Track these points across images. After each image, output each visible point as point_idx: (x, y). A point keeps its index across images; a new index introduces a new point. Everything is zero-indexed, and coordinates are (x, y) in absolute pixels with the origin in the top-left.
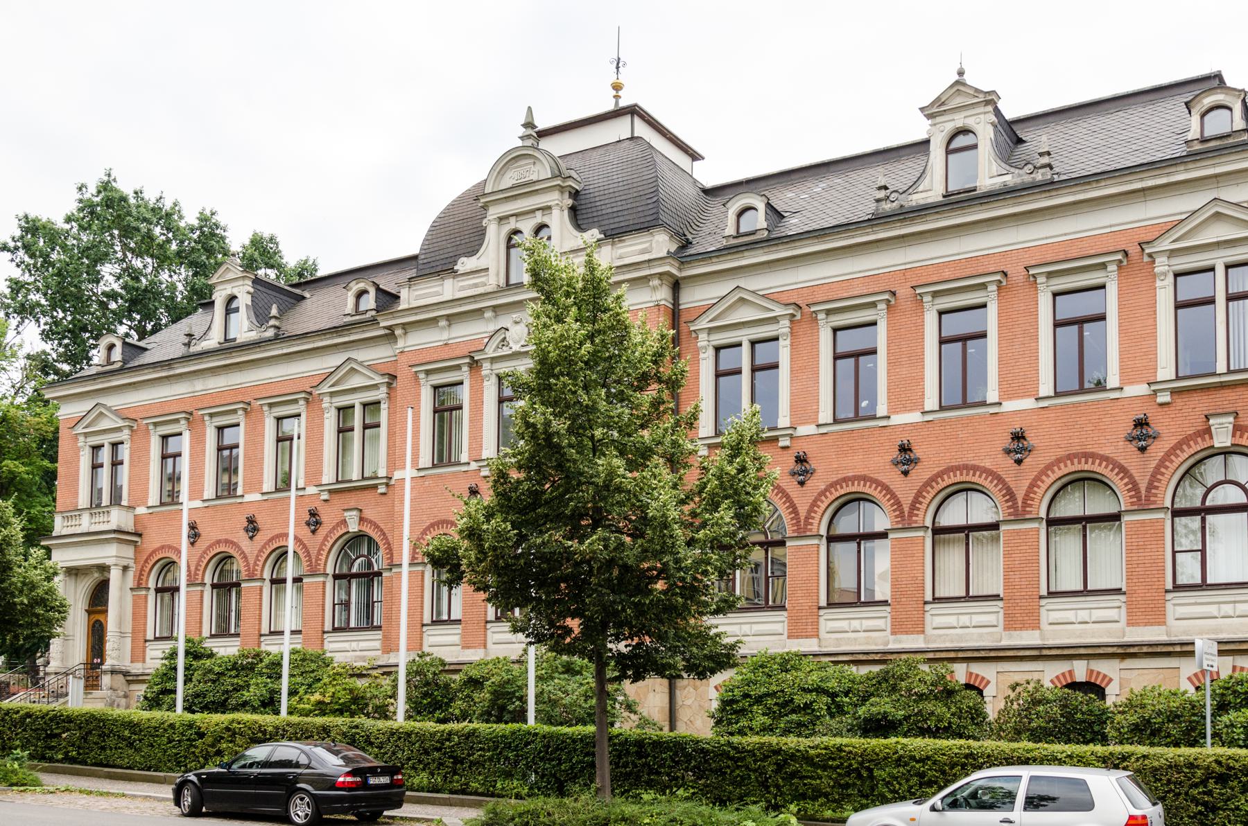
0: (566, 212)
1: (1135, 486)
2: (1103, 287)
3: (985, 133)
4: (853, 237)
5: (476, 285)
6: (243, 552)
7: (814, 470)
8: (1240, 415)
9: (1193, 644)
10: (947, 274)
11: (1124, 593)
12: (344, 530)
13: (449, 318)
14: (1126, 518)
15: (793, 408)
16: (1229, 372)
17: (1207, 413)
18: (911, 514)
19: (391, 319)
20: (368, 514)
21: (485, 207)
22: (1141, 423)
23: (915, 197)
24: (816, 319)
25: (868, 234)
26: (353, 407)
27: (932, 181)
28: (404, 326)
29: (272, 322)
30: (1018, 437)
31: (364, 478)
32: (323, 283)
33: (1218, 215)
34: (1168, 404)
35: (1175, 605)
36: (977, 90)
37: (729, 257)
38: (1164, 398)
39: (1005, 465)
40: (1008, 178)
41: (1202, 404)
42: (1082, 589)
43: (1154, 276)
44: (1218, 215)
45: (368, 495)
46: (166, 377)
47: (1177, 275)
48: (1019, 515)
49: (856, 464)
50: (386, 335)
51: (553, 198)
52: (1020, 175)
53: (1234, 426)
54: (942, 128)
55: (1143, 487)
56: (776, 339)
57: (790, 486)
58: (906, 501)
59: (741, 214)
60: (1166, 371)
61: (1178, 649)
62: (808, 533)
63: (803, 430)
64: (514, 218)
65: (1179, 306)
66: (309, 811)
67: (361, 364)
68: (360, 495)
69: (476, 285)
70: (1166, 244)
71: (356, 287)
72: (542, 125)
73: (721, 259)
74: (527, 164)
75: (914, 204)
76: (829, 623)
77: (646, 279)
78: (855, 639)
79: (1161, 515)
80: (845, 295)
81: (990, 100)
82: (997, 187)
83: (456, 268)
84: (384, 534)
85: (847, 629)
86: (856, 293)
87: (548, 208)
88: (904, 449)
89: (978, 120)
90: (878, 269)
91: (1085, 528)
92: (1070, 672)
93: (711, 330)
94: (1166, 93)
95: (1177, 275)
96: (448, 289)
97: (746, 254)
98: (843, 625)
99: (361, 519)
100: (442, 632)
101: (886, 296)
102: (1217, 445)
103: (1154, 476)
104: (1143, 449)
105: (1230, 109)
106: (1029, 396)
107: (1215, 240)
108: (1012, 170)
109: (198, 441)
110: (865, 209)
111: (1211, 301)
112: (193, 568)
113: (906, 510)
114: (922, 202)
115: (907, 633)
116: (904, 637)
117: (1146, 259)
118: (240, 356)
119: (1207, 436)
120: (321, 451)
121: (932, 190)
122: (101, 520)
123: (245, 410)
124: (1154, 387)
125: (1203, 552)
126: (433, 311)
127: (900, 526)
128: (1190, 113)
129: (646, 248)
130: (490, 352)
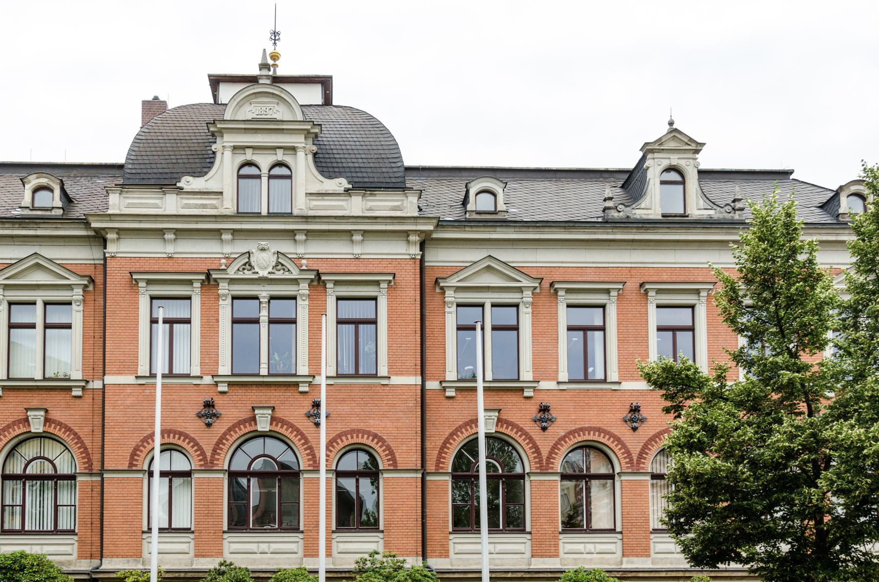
1: (203, 454)
2: (189, 298)
4: (595, 233)
5: (204, 206)
7: (221, 414)
8: (276, 410)
9: (481, 572)
10: (665, 278)
11: (193, 532)
12: (252, 429)
13: (178, 232)
14: (195, 476)
15: (536, 367)
16: (270, 375)
17: (253, 405)
18: (639, 462)
19: (107, 221)
20: (55, 415)
21: (221, 132)
22: (209, 405)
23: (638, 212)
25: (608, 233)
27: (651, 201)
28: (119, 231)
30: (635, 410)
31: (45, 379)
32: (710, 176)
33: (38, 265)
34: (305, 393)
35: (230, 542)
36: (691, 140)
37: (482, 229)
38: (223, 388)
40: (712, 212)
43: (218, 296)
44: (38, 265)
45: (58, 397)
48: (208, 466)
49: (591, 418)
50: (88, 237)
51: (298, 140)
52: (721, 213)
53: (272, 417)
54: (659, 163)
55: (209, 454)
57: (534, 430)
58: (635, 452)
60: (224, 369)
62: (550, 471)
63: (544, 385)
64: (282, 150)
65: (235, 321)
68: (44, 395)
69: (204, 206)
70: (453, 282)
71: (34, 181)
72: (282, 71)
73: (474, 229)
74: (273, 103)
75: (638, 217)
77: (407, 233)
78: (591, 560)
80: (580, 279)
82: (705, 217)
83: (178, 185)
84: (79, 438)
85: (256, 551)
86: (589, 279)
87: (293, 149)
88: (635, 410)
89: (688, 163)
90: (609, 263)
93: (458, 289)
94: (756, 177)
95: (234, 298)
96: (170, 204)
97: (498, 229)
98: (253, 547)
99: (47, 420)
100: (345, 540)
102: (259, 429)
104: (209, 425)
105: (494, 195)
108: (715, 207)
109: (317, 313)
110: (594, 212)
111: (256, 321)
113: (635, 458)
114: (645, 217)
115: (637, 556)
116: (635, 559)
117: (438, 290)
118: (64, 229)
119: (253, 423)
124: (216, 379)
126: (162, 222)
127: (630, 471)
128: (24, 186)
129: (398, 206)
130: (232, 273)
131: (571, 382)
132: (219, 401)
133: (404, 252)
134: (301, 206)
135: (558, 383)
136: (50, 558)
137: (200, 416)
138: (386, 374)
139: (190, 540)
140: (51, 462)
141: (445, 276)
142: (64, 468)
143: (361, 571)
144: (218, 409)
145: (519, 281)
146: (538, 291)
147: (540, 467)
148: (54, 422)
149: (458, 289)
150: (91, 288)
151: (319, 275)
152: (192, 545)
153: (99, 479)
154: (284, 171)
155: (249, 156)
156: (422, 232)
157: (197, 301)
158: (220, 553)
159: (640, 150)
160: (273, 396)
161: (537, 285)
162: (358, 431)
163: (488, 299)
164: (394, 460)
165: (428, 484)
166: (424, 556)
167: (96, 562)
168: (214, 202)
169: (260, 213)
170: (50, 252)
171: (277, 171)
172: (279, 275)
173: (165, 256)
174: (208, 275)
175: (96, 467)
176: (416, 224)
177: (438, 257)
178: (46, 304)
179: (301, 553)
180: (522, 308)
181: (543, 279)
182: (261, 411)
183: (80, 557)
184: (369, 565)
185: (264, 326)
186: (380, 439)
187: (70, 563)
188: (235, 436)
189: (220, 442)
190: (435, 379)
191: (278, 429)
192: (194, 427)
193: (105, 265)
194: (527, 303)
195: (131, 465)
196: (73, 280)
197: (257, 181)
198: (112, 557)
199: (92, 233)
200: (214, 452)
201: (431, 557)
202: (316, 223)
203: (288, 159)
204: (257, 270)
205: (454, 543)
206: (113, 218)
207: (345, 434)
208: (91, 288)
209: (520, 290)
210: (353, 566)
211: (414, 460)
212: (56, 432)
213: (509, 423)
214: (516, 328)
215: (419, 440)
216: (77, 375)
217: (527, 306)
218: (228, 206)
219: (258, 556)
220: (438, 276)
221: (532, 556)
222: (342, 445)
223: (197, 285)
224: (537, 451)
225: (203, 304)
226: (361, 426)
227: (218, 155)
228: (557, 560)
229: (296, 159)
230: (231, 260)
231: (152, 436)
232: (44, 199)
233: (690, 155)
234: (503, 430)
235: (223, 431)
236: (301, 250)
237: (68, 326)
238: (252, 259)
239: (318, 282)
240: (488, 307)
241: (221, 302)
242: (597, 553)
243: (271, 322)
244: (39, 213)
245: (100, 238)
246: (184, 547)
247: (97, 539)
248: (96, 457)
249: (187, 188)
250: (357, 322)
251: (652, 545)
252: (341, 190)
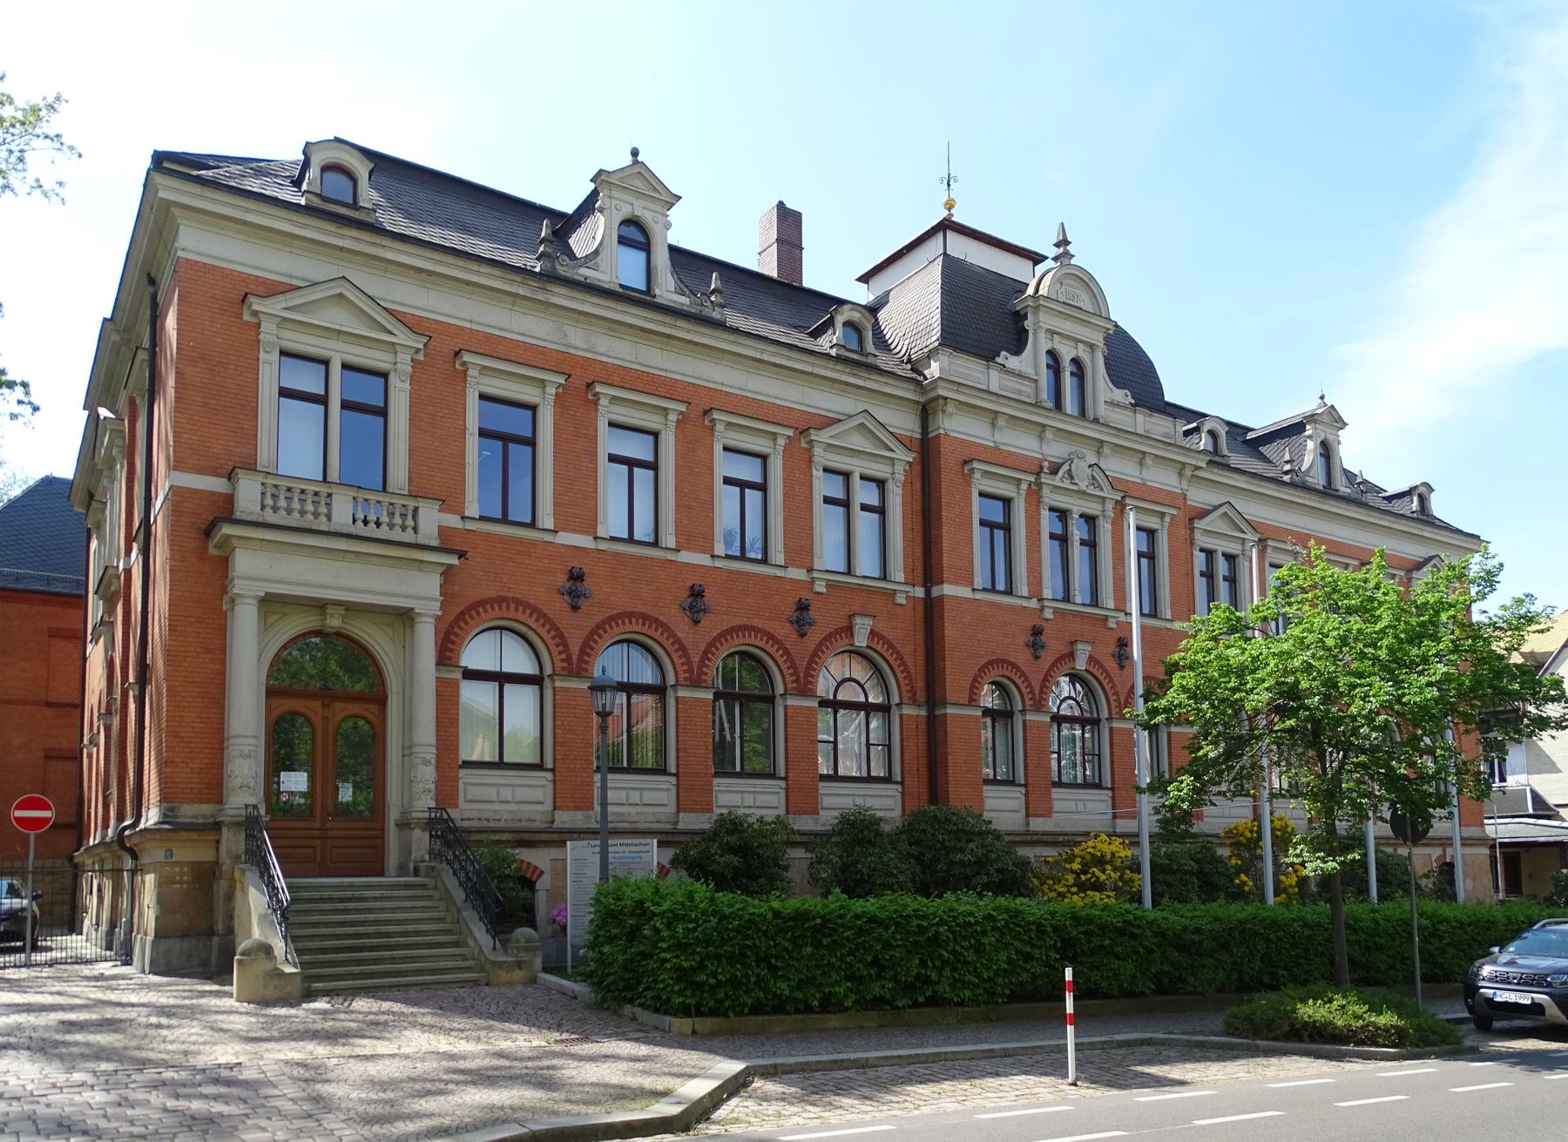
6: (678, 641)
34: (822, 594)
39: (557, 607)
42: (497, 760)
46: (835, 381)
55: (575, 650)
57: (682, 627)
103: (706, 652)
105: (354, 180)
106: (803, 567)
107: (338, 328)
131: (482, 518)
139: (545, 783)
145: (1244, 532)
159: (591, 181)
161: (421, 346)
173: (992, 444)
181: (570, 376)
205: (465, 784)
206: (960, 389)
214: (382, 412)
217: (403, 378)
220: (247, 291)
233: (658, 208)
240: (336, 369)
242: (644, 805)
251: (461, 786)
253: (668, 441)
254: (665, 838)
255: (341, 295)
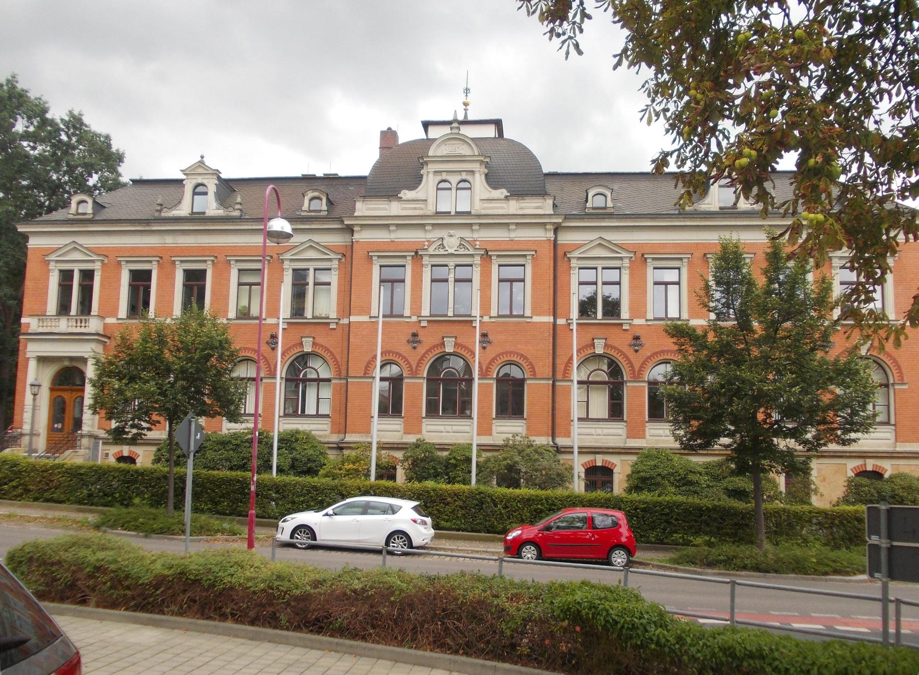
0: (483, 176)
1: (410, 366)
2: (404, 266)
3: (212, 188)
5: (415, 209)
12: (592, 351)
13: (397, 225)
15: (632, 309)
16: (455, 316)
20: (319, 340)
22: (415, 335)
24: (175, 264)
26: (309, 270)
28: (362, 226)
29: (238, 206)
33: (75, 248)
34: (425, 327)
38: (424, 324)
41: (444, 329)
43: (422, 266)
44: (311, 246)
47: (432, 266)
50: (342, 229)
51: (476, 167)
55: (414, 367)
56: (330, 269)
57: (630, 352)
59: (311, 199)
60: (426, 312)
61: (611, 451)
63: (637, 322)
65: (433, 281)
66: (535, 552)
67: (81, 245)
69: (415, 209)
76: (498, 428)
77: (545, 224)
78: (668, 441)
79: (421, 381)
81: (216, 173)
84: (333, 355)
87: (473, 172)
91: (588, 387)
92: (122, 451)
93: (579, 258)
95: (432, 266)
96: (394, 208)
98: (442, 428)
99: (314, 344)
100: (615, 427)
101: (212, 258)
104: (415, 348)
105: (606, 196)
111: (446, 281)
112: (484, 368)
114: (707, 210)
117: (566, 259)
120: (279, 296)
121: (184, 210)
122: (49, 324)
123: (213, 261)
125: (588, 402)
126: (388, 220)
130: (431, 251)
132: (421, 333)
133: (543, 235)
134: (478, 208)
135: (490, 317)
136: (313, 433)
137: (408, 341)
138: (530, 315)
140: (316, 370)
141: (571, 250)
142: (324, 374)
143: (506, 446)
144: (420, 338)
146: (633, 259)
147: (412, 374)
148: (318, 345)
149: (579, 258)
150: (343, 260)
151: (487, 251)
152: (402, 426)
153: (345, 382)
154: (466, 185)
155: (444, 176)
156: (554, 223)
157: (409, 269)
158: (420, 432)
160: (457, 329)
162: (511, 353)
163: (600, 264)
164: (902, 379)
165: (557, 387)
166: (553, 436)
167: (342, 436)
168: (421, 206)
169: (204, 213)
170: (317, 238)
171: (462, 185)
172: (462, 252)
173: (545, 239)
174: (416, 253)
175: (344, 373)
176: (550, 218)
177: (565, 238)
178: (315, 270)
179: (624, 436)
180: (623, 271)
182: (448, 339)
183: (332, 432)
184: (511, 442)
185: (451, 283)
186: (525, 358)
187: (325, 436)
188: (431, 355)
189: (422, 359)
190: (563, 318)
191: (459, 351)
192: (405, 349)
193: (352, 246)
194: (626, 267)
195: (365, 373)
196: (332, 256)
197: (449, 192)
198: (352, 432)
199: (345, 227)
200: (418, 366)
201: (559, 437)
202: (484, 219)
203: (469, 178)
204: (447, 248)
207: (502, 354)
208: (343, 260)
209: (621, 259)
210: (501, 443)
211: (548, 372)
212: (319, 351)
213: (612, 347)
214: (619, 283)
215: (551, 359)
216: (333, 315)
218: (431, 209)
219: (444, 434)
220: (565, 250)
221: (628, 438)
222: (500, 361)
223: (409, 258)
224: (632, 366)
225: (413, 270)
226: (512, 349)
227: (425, 177)
228: (644, 441)
229: (474, 177)
230: (431, 243)
231: (375, 357)
232: (316, 205)
234: (609, 352)
235: (423, 352)
236: (476, 235)
237: (329, 284)
238: (445, 242)
239: (487, 256)
240: (600, 269)
241: (424, 269)
243: (456, 281)
244: (313, 214)
245: (350, 230)
246: (397, 427)
247: (343, 421)
248: (344, 368)
249: (404, 198)
250: (511, 281)
252: (503, 197)
253: (684, 271)
254: (105, 441)
255: (600, 244)
